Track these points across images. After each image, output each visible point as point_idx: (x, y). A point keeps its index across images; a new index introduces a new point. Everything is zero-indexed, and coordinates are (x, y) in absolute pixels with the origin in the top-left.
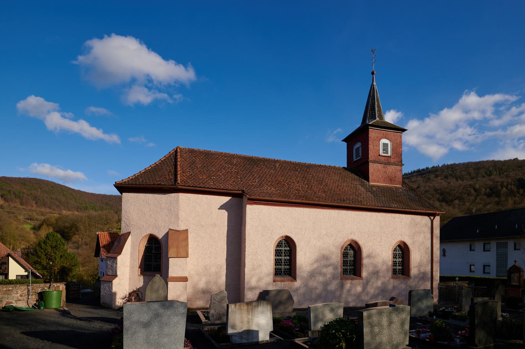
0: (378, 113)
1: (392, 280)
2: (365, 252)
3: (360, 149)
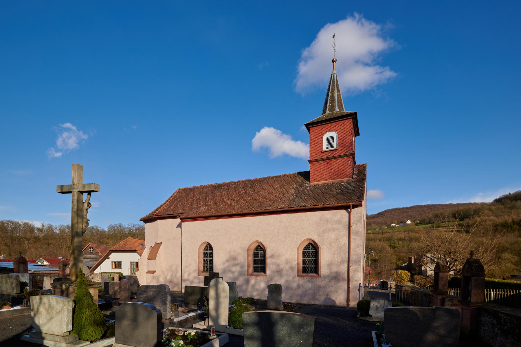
0: (329, 105)
1: (297, 278)
2: (269, 253)
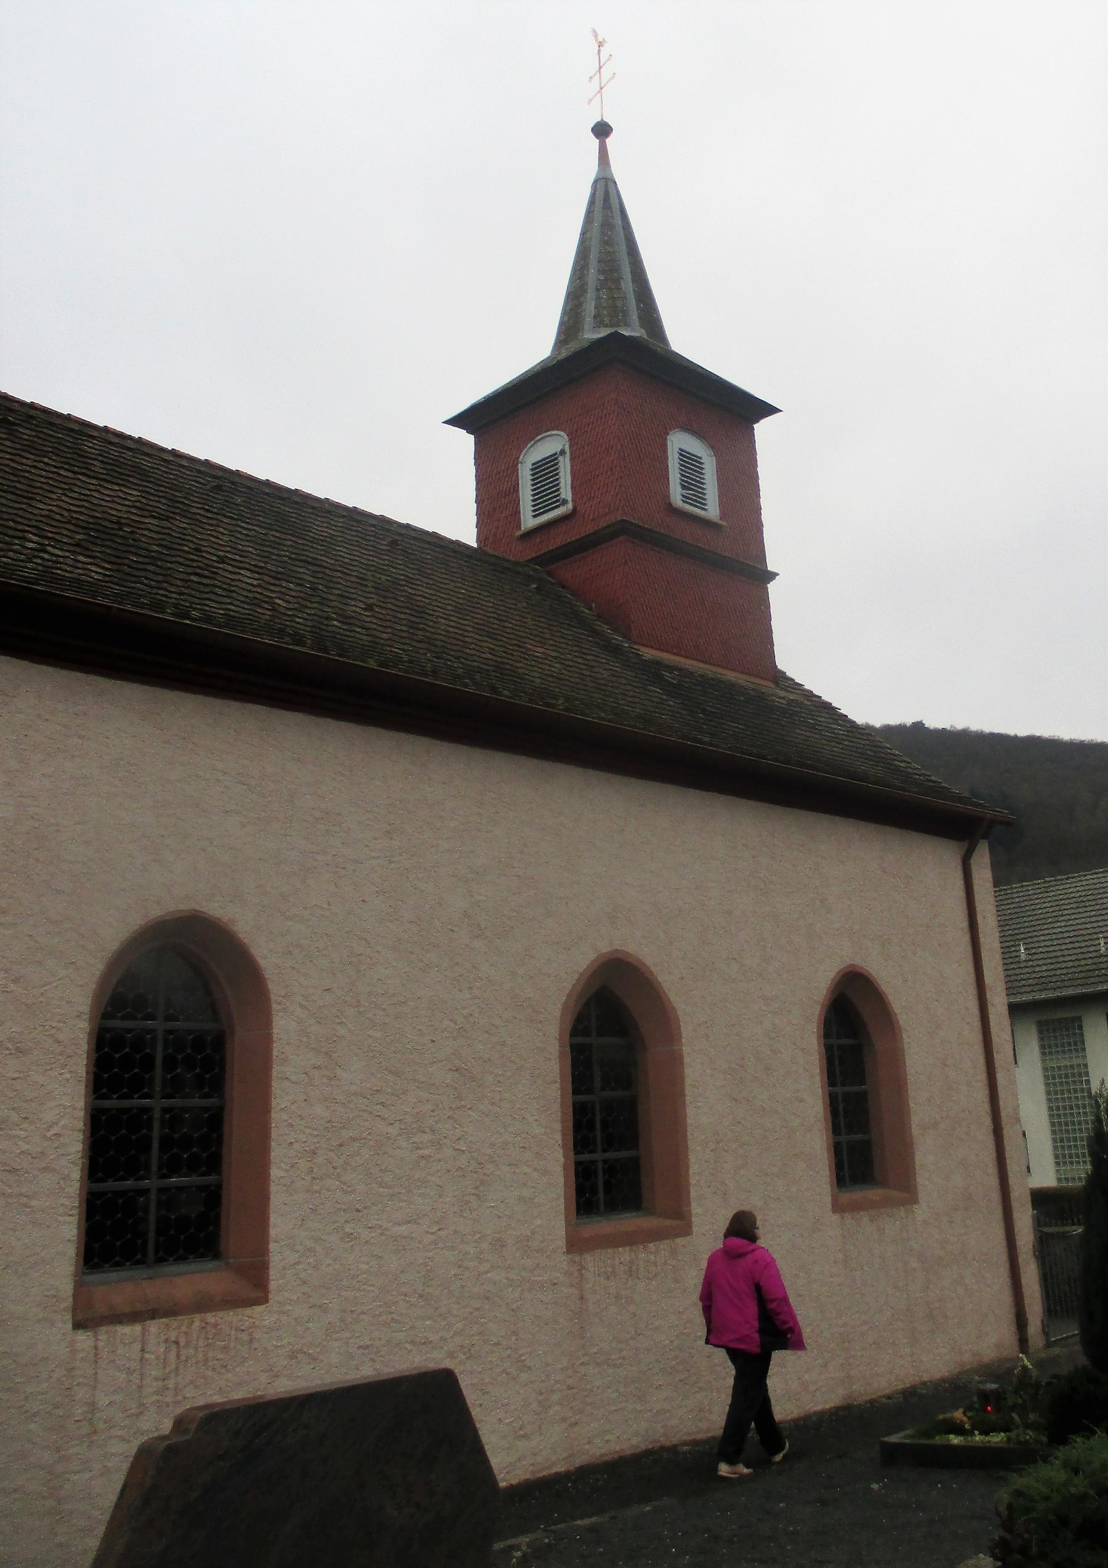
3: (565, 467)
